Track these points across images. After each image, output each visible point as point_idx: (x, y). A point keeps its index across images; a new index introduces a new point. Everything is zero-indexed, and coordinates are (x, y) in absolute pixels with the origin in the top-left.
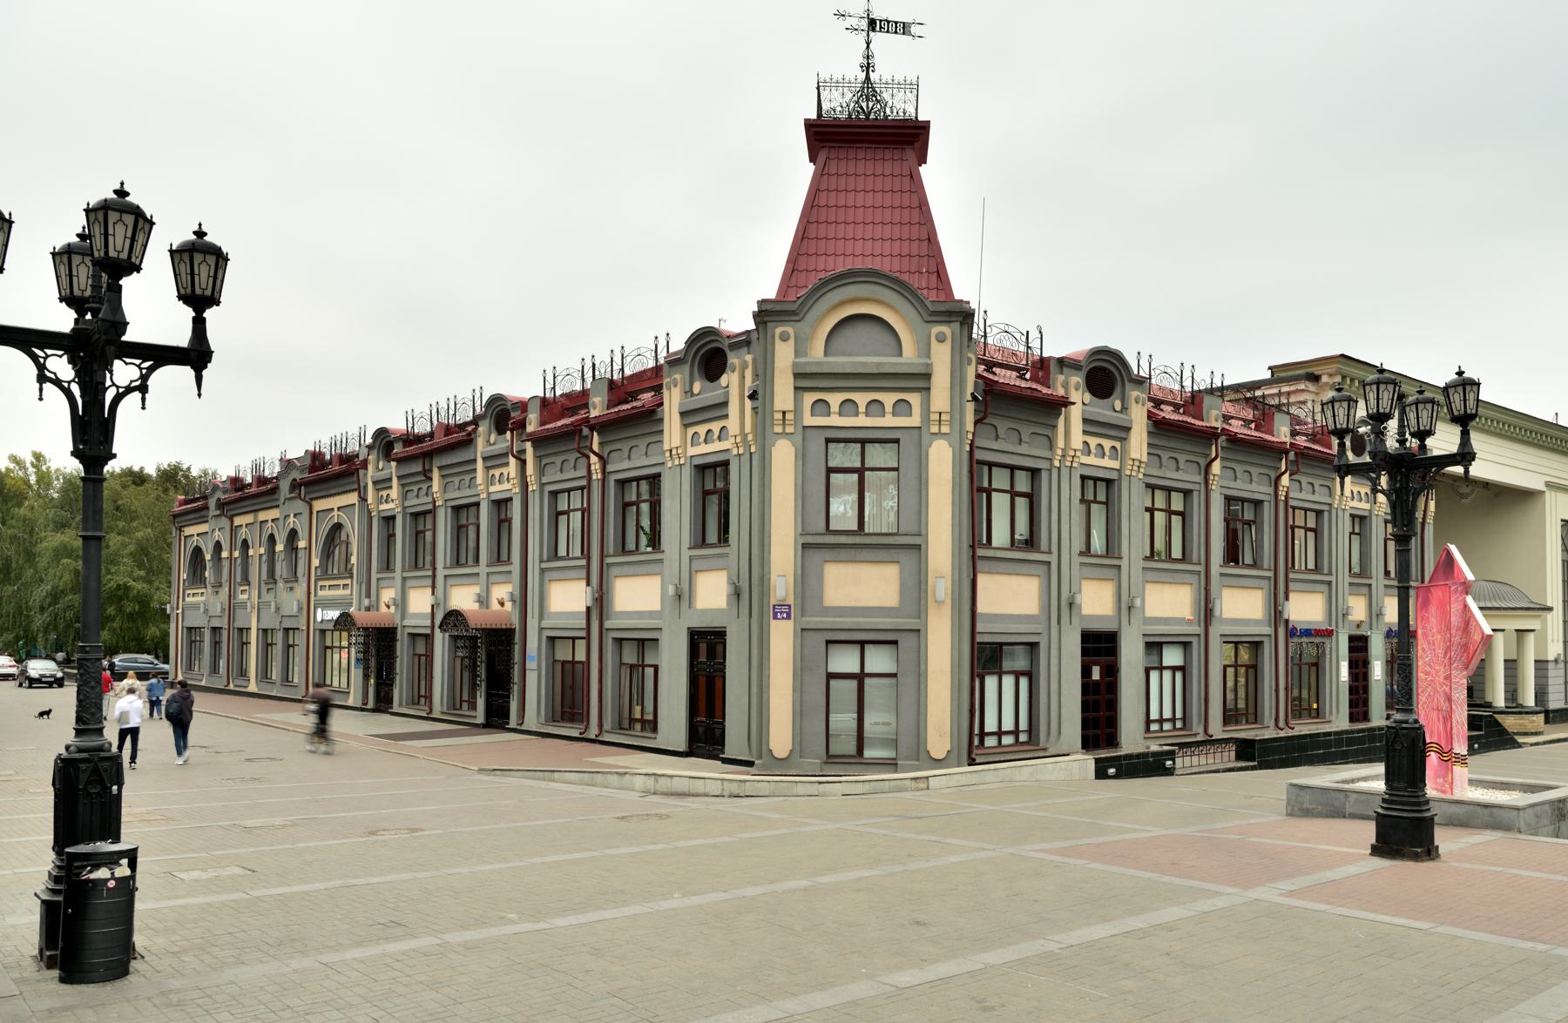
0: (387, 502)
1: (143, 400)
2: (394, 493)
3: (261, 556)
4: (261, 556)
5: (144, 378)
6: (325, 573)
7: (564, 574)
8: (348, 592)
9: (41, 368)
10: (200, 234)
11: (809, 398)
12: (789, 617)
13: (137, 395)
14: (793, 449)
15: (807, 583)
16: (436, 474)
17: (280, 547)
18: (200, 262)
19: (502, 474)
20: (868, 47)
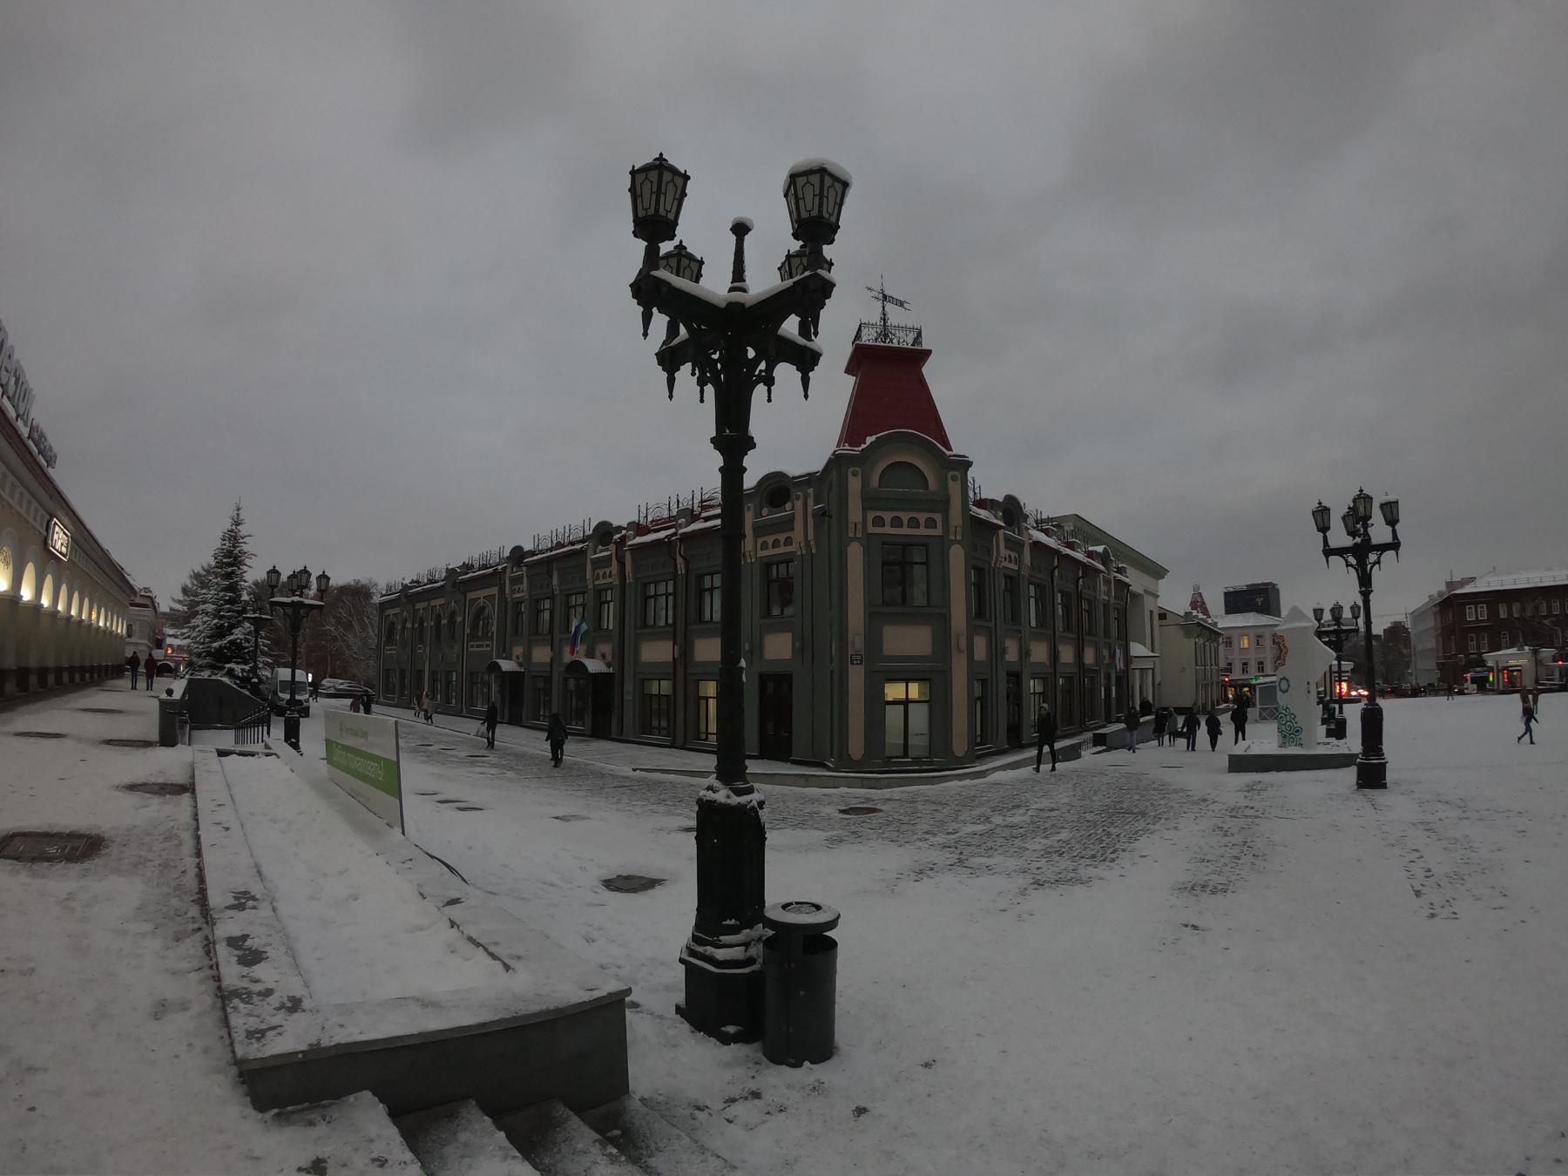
0: (518, 592)
1: (769, 392)
2: (525, 586)
3: (431, 627)
4: (431, 627)
5: (1379, 558)
6: (473, 636)
7: (657, 635)
8: (489, 649)
9: (1347, 561)
10: (1361, 491)
11: (871, 515)
12: (861, 663)
13: (1377, 565)
14: (862, 549)
15: (873, 638)
16: (555, 574)
17: (444, 622)
18: (803, 184)
19: (605, 573)
20: (884, 309)
